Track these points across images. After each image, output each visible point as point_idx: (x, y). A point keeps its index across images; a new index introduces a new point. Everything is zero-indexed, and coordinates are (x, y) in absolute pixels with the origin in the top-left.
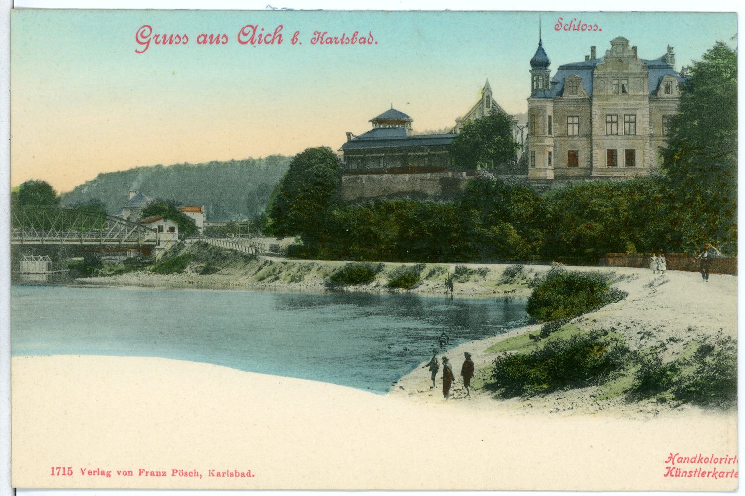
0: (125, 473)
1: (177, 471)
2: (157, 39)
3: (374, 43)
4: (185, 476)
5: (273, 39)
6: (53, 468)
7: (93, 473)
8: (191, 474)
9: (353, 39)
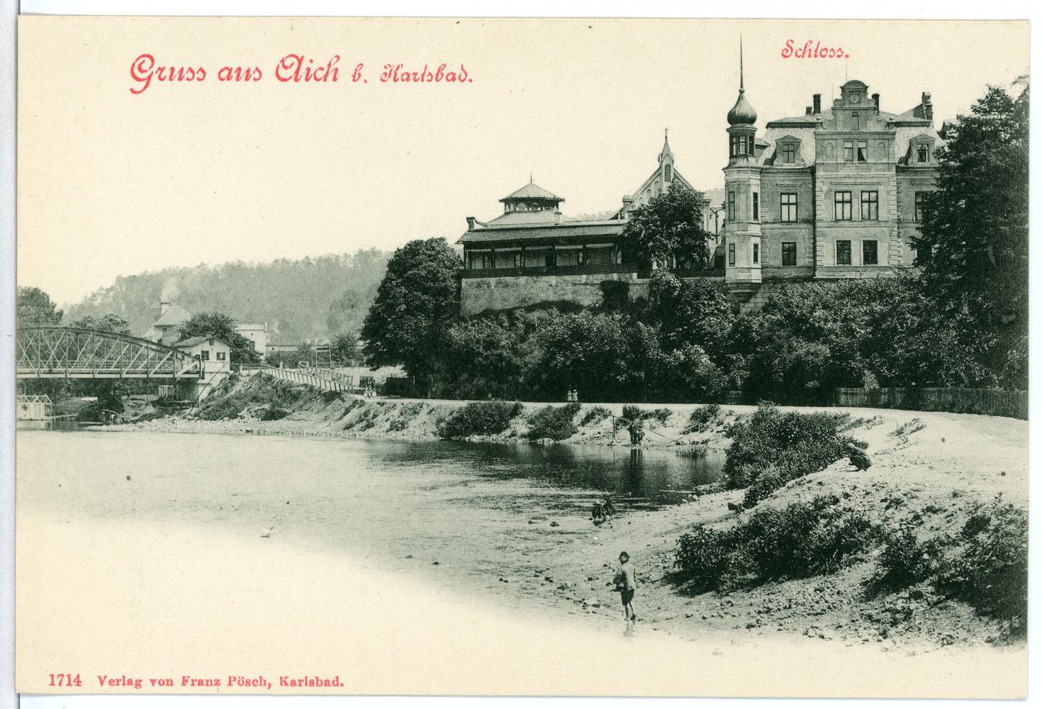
0: (162, 683)
2: (161, 73)
7: (116, 683)
8: (255, 683)
9: (437, 75)
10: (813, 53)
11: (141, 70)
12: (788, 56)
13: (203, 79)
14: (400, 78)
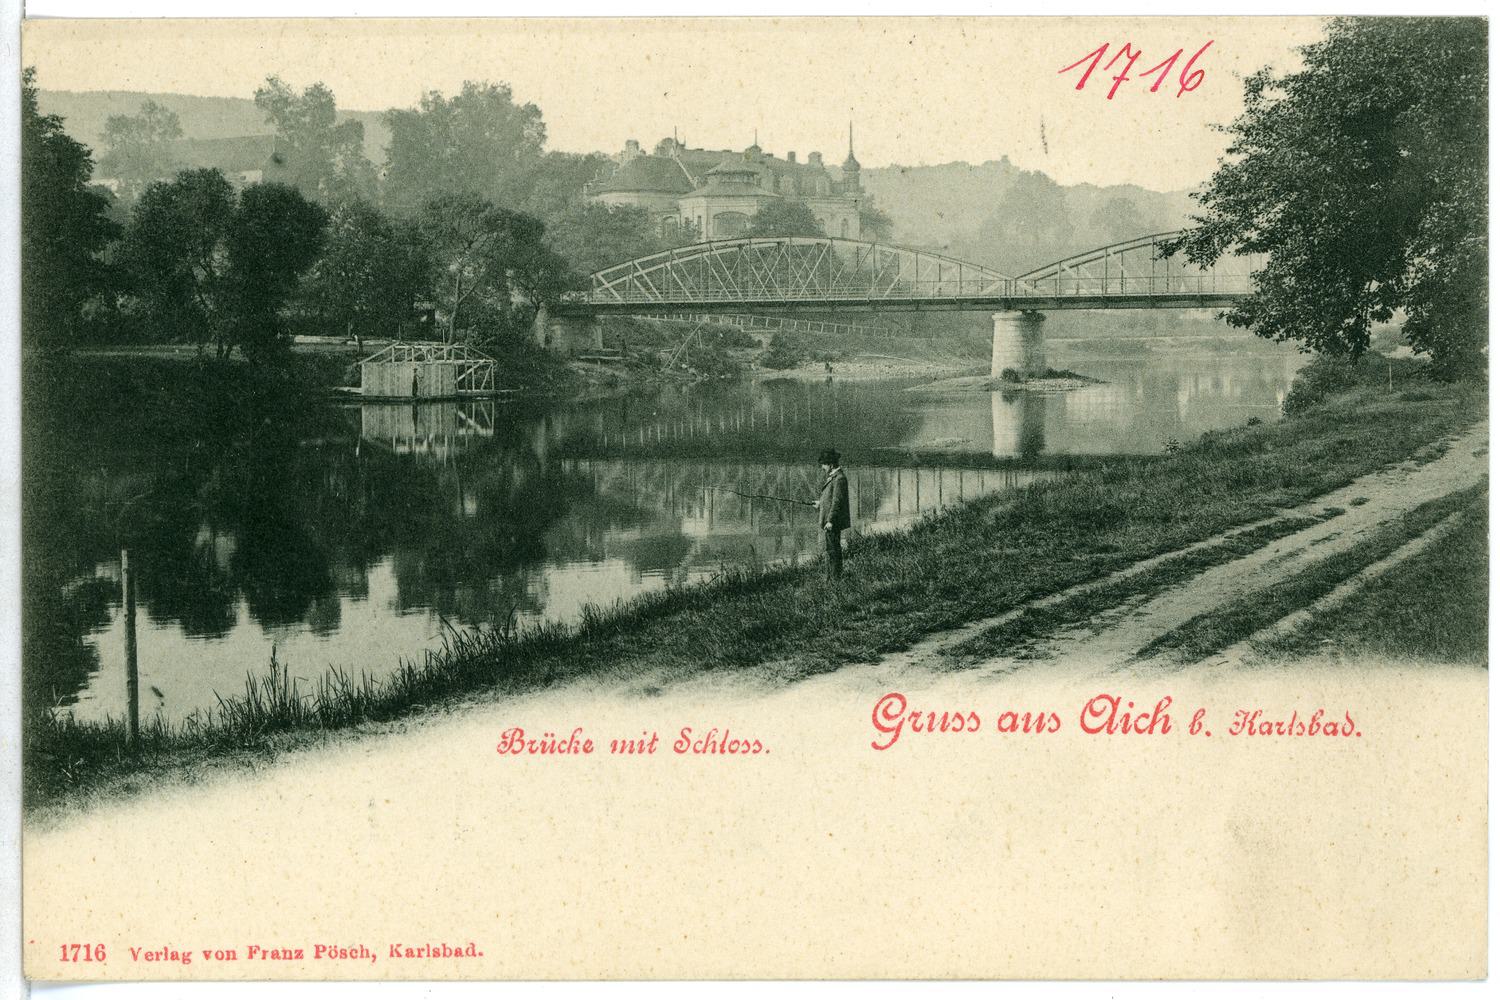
0: (220, 955)
1: (324, 948)
2: (915, 722)
3: (1354, 733)
4: (341, 957)
5: (1154, 723)
6: (64, 947)
7: (155, 957)
8: (354, 954)
9: (1311, 727)
10: (718, 748)
11: (887, 716)
12: (683, 752)
13: (977, 728)
14: (1258, 731)
